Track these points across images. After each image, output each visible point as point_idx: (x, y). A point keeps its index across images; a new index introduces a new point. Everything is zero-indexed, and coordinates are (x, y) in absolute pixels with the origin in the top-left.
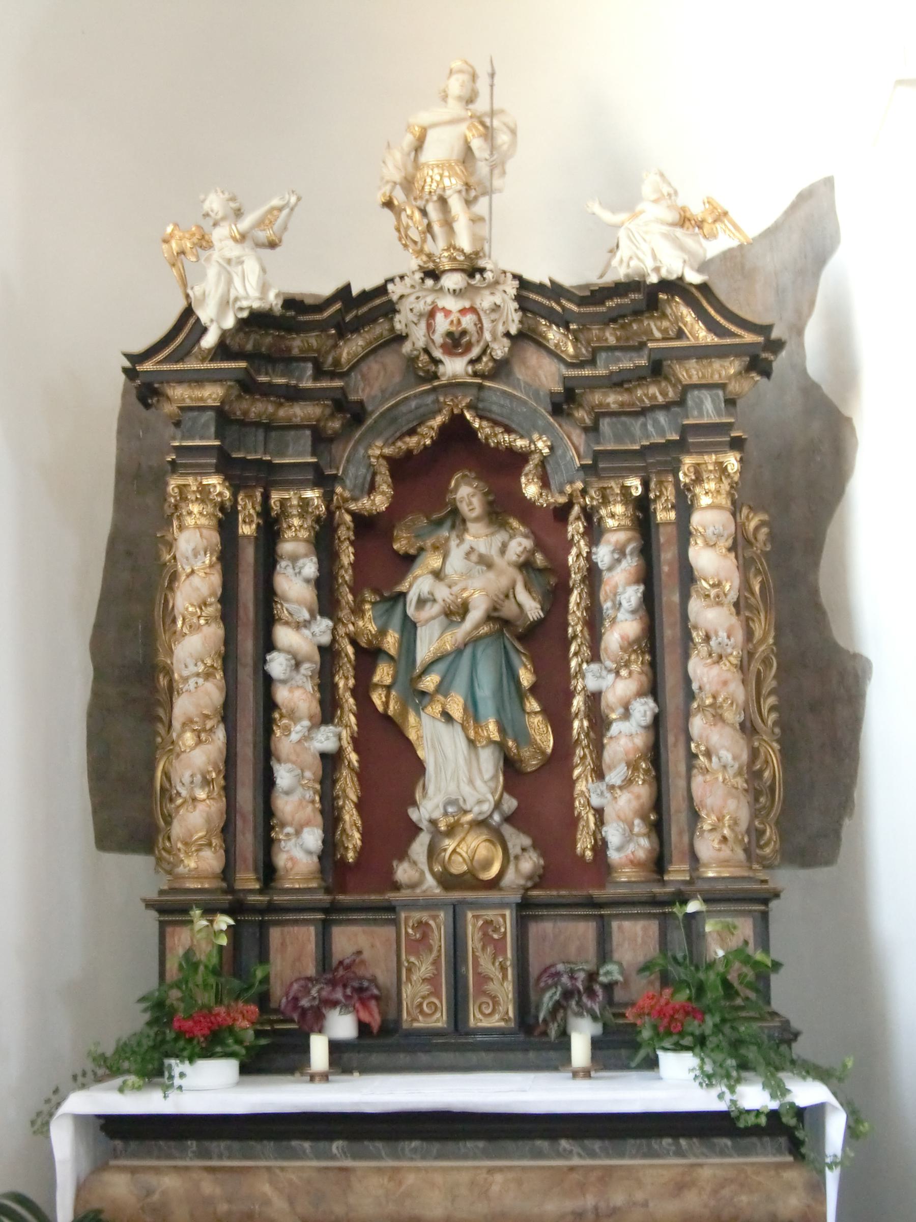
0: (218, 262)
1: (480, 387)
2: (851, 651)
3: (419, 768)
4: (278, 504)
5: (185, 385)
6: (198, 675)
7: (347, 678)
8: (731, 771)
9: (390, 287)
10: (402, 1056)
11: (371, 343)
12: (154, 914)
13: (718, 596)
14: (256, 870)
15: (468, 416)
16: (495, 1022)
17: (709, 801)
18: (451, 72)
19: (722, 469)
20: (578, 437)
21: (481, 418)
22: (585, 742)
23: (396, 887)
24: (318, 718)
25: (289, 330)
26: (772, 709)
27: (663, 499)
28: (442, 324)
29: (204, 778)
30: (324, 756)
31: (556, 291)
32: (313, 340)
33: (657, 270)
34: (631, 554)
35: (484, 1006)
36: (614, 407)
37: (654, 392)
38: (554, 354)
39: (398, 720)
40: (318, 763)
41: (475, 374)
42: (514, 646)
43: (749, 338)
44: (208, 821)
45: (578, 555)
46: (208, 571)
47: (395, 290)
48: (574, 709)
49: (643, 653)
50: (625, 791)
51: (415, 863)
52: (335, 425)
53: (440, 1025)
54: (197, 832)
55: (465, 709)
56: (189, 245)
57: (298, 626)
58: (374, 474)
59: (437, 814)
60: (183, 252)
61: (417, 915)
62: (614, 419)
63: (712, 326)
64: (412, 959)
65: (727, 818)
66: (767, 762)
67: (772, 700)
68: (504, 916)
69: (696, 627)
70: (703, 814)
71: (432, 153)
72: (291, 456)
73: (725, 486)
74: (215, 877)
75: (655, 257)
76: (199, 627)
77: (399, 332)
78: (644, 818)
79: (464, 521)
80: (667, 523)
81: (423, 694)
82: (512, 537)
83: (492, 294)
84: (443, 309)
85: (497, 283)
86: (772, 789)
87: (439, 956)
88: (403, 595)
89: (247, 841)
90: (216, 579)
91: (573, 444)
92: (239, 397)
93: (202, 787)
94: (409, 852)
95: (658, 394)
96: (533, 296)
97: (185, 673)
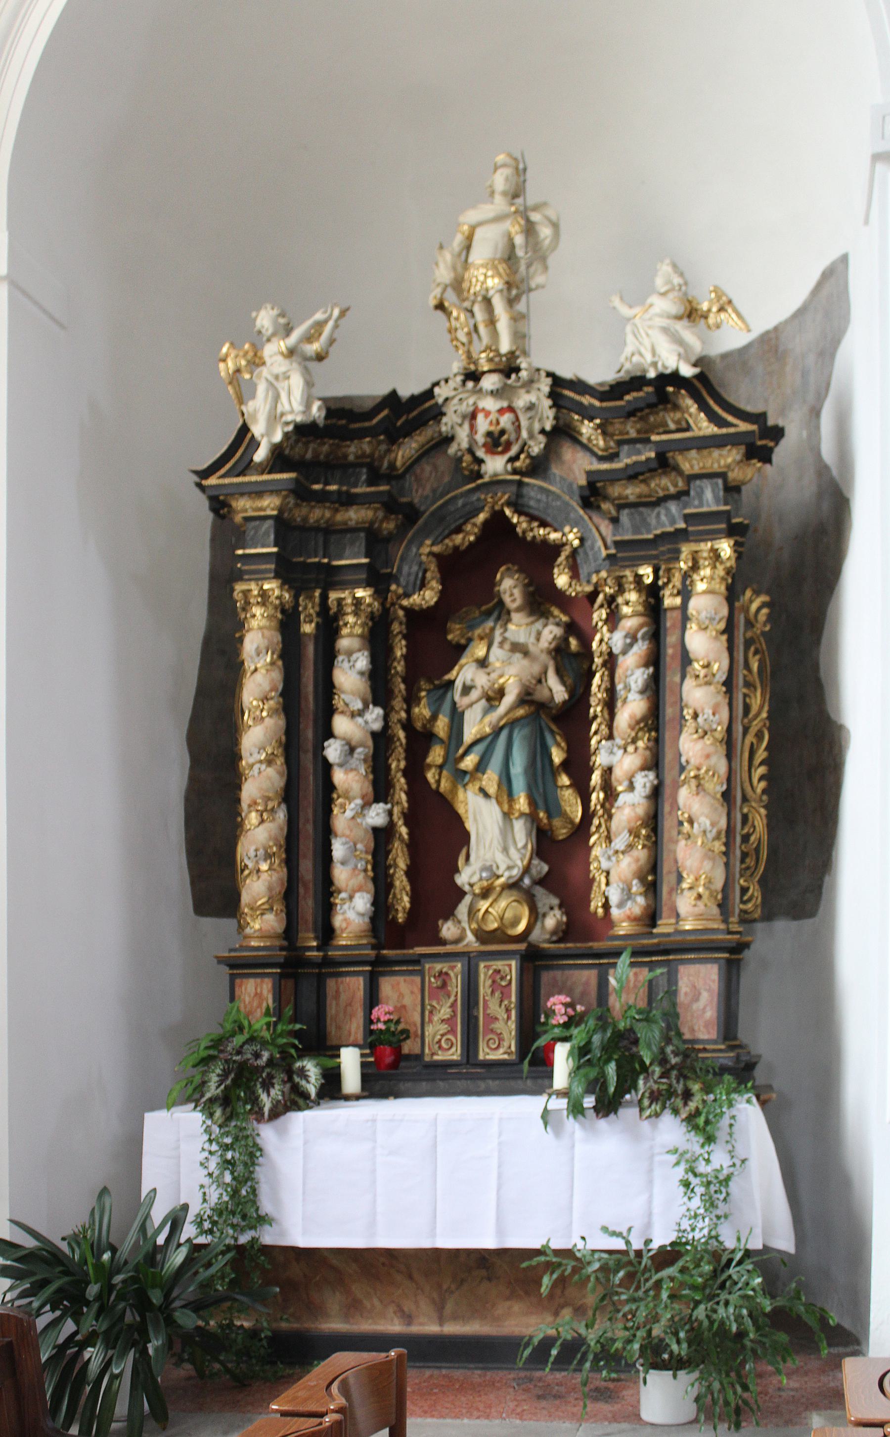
0: (267, 380)
1: (520, 484)
2: (839, 723)
3: (464, 838)
4: (335, 602)
5: (246, 498)
6: (261, 762)
7: (399, 761)
8: (710, 836)
9: (437, 390)
10: (424, 1083)
11: (423, 446)
12: (226, 970)
13: (706, 676)
14: (315, 931)
15: (508, 512)
16: (499, 1055)
17: (688, 863)
18: (496, 169)
19: (716, 555)
20: (606, 528)
21: (520, 513)
22: (601, 812)
23: (443, 942)
24: (371, 797)
25: (344, 438)
26: (761, 778)
27: (670, 586)
28: (483, 425)
29: (266, 852)
30: (376, 830)
31: (579, 386)
32: (366, 445)
33: (654, 364)
34: (643, 638)
35: (491, 1041)
36: (632, 499)
37: (665, 484)
38: (586, 448)
39: (449, 797)
40: (370, 836)
41: (515, 472)
42: (547, 724)
43: (744, 427)
44: (270, 889)
45: (601, 641)
46: (269, 667)
47: (441, 393)
48: (593, 783)
49: (650, 731)
50: (626, 855)
51: (459, 922)
52: (389, 526)
53: (455, 1057)
54: (260, 899)
55: (499, 785)
56: (243, 363)
57: (353, 715)
58: (425, 571)
59: (475, 879)
60: (238, 371)
61: (438, 967)
62: (633, 510)
63: (713, 418)
64: (434, 1003)
65: (703, 877)
66: (754, 827)
67: (762, 770)
68: (510, 966)
69: (687, 706)
70: (685, 875)
71: (480, 254)
72: (347, 559)
73: (720, 571)
74: (277, 936)
75: (654, 353)
76: (262, 719)
77: (444, 434)
78: (642, 879)
79: (509, 612)
80: (673, 609)
81: (465, 773)
82: (545, 625)
83: (528, 392)
84: (483, 410)
85: (531, 381)
86: (757, 850)
87: (456, 1001)
88: (451, 683)
89: (308, 906)
90: (277, 676)
91: (601, 534)
92: (297, 505)
93: (265, 860)
94: (456, 912)
95: (669, 485)
96: (568, 393)
97: (251, 760)
